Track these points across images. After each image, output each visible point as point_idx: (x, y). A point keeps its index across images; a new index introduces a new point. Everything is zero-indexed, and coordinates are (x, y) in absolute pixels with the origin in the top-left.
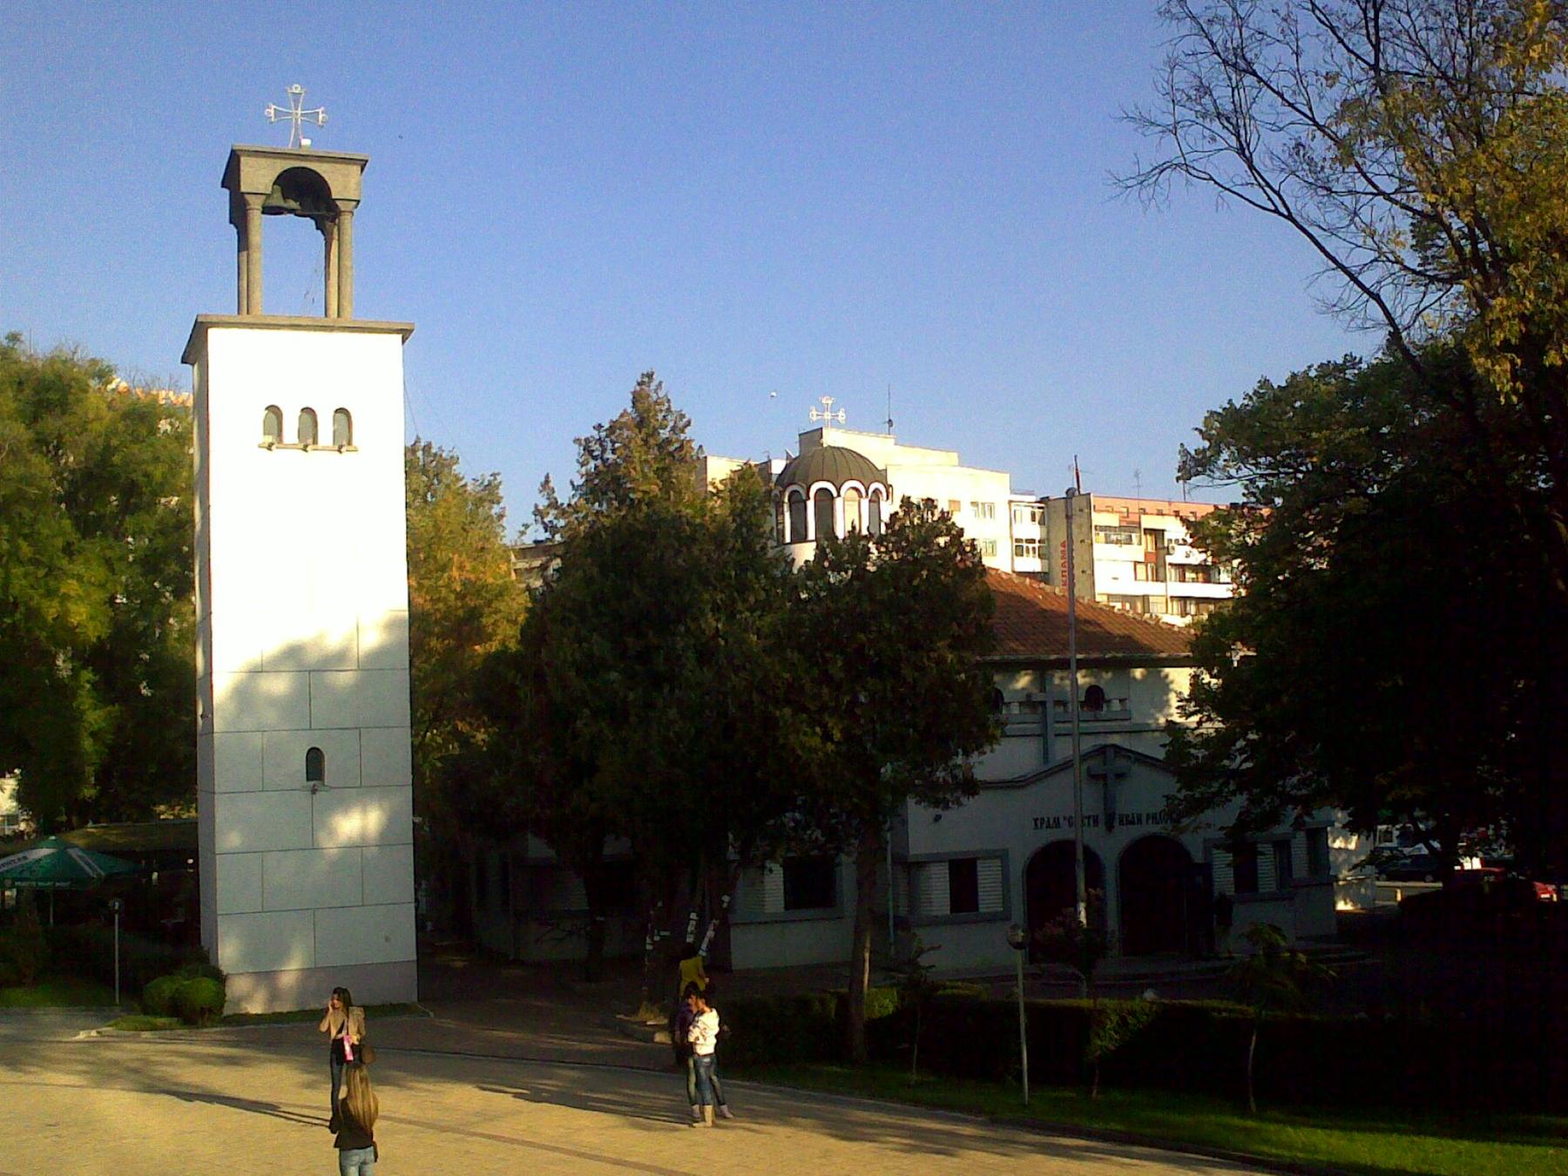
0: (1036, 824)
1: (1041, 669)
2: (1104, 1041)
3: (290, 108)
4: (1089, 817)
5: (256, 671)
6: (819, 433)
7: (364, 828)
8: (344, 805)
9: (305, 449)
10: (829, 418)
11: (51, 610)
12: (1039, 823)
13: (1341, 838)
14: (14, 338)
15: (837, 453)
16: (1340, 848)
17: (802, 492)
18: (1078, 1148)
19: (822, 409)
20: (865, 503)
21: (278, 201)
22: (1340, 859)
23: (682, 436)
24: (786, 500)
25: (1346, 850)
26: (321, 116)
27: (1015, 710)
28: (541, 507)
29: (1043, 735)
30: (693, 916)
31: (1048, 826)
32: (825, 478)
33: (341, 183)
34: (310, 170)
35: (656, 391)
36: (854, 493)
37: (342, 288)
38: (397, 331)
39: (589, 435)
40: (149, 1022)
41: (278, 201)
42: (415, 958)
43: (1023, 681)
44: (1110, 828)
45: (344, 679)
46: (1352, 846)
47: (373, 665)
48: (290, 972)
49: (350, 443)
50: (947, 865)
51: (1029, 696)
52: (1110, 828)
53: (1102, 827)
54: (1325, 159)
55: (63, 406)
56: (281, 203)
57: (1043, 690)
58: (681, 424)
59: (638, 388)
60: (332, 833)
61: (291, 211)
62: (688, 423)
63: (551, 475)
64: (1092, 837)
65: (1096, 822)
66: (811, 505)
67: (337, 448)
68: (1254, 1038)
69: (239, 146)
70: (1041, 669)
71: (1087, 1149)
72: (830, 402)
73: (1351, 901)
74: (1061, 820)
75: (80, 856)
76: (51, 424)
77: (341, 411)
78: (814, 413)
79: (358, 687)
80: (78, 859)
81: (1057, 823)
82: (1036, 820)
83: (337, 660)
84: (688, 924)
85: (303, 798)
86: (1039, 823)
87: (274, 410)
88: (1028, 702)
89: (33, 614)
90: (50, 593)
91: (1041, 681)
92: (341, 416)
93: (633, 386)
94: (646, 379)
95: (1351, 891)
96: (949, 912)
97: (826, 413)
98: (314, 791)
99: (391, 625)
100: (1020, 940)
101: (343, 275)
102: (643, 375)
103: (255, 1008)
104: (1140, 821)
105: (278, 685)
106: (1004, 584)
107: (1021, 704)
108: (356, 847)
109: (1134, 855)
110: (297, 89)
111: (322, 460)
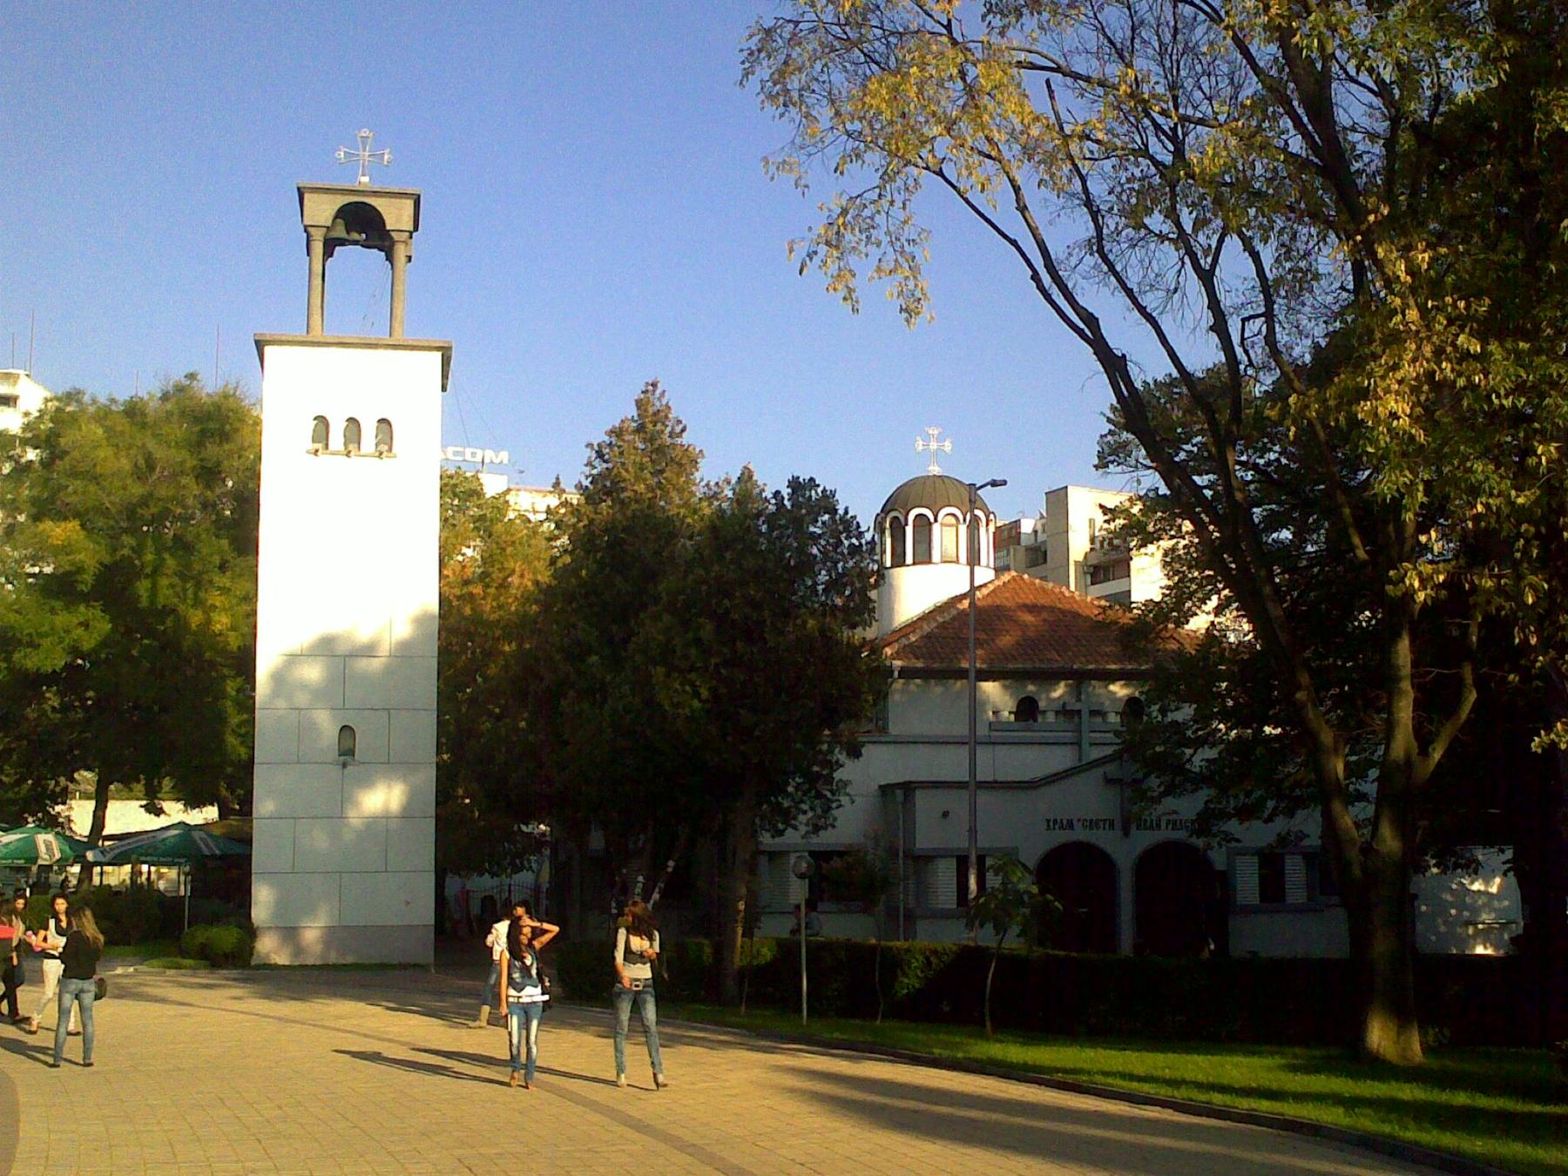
0: (1048, 826)
1: (1079, 678)
2: (910, 982)
3: (358, 150)
4: (1105, 820)
5: (293, 659)
6: (1064, 491)
7: (387, 802)
8: (367, 782)
9: (348, 454)
10: (932, 443)
11: (195, 618)
12: (1051, 824)
13: (1480, 881)
14: (192, 376)
15: (939, 481)
16: (1479, 891)
17: (902, 519)
18: (769, 1047)
19: (927, 439)
20: (963, 529)
21: (340, 232)
22: (1480, 902)
23: (679, 441)
24: (888, 525)
25: (1487, 893)
26: (386, 157)
27: (1051, 717)
28: (552, 507)
29: (1078, 744)
30: (641, 879)
31: (1062, 827)
32: (924, 503)
33: (396, 216)
34: (370, 205)
35: (659, 399)
36: (952, 520)
37: (394, 310)
38: (438, 349)
39: (600, 441)
40: (176, 963)
41: (340, 232)
42: (433, 922)
43: (1059, 691)
44: (1126, 833)
45: (376, 664)
46: (1494, 889)
47: (404, 652)
48: (312, 934)
49: (390, 450)
50: (954, 861)
51: (1064, 705)
52: (1126, 833)
53: (1119, 832)
54: (1037, 119)
55: (224, 437)
56: (343, 235)
57: (1079, 700)
58: (678, 429)
59: (642, 396)
60: (356, 804)
61: (356, 243)
62: (683, 430)
63: (560, 477)
64: (1107, 840)
65: (1112, 825)
66: (909, 530)
67: (377, 454)
68: (993, 965)
69: (303, 183)
70: (1079, 678)
71: (800, 1050)
72: (936, 432)
73: (1491, 945)
74: (1075, 822)
75: (201, 838)
76: (212, 451)
77: (383, 421)
78: (921, 443)
79: (389, 671)
80: (199, 841)
81: (1070, 825)
82: (1048, 821)
83: (368, 651)
84: (635, 886)
85: (335, 771)
86: (1052, 824)
87: (322, 421)
88: (1064, 712)
89: (182, 624)
90: (198, 602)
91: (1077, 691)
92: (384, 426)
93: (637, 394)
94: (650, 388)
95: (1492, 936)
96: (955, 906)
97: (935, 447)
98: (344, 765)
99: (420, 621)
100: (803, 870)
101: (395, 299)
102: (647, 383)
103: (282, 959)
104: (1159, 826)
105: (312, 673)
106: (1064, 601)
107: (1057, 713)
108: (377, 823)
109: (1153, 862)
110: (365, 132)
111: (363, 467)
